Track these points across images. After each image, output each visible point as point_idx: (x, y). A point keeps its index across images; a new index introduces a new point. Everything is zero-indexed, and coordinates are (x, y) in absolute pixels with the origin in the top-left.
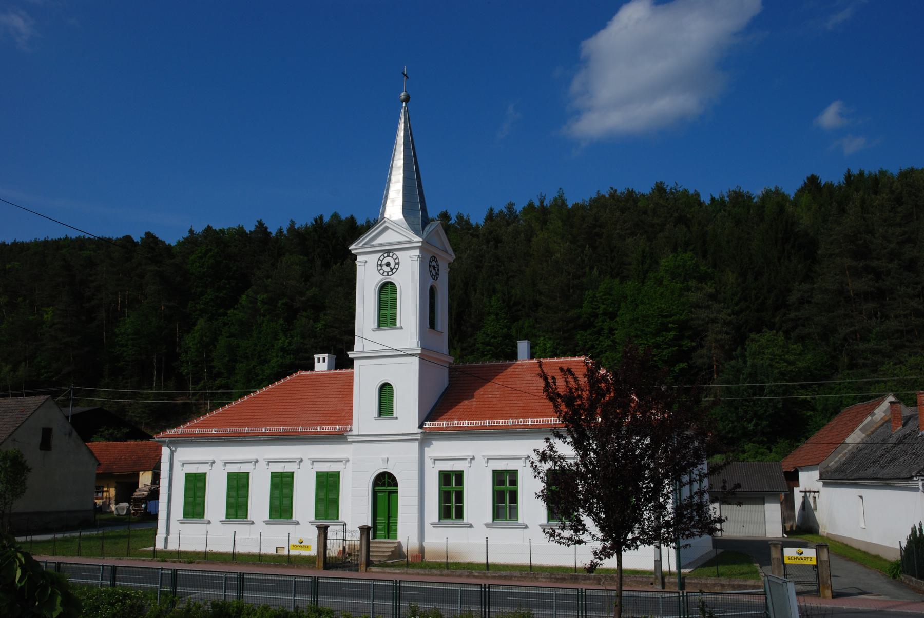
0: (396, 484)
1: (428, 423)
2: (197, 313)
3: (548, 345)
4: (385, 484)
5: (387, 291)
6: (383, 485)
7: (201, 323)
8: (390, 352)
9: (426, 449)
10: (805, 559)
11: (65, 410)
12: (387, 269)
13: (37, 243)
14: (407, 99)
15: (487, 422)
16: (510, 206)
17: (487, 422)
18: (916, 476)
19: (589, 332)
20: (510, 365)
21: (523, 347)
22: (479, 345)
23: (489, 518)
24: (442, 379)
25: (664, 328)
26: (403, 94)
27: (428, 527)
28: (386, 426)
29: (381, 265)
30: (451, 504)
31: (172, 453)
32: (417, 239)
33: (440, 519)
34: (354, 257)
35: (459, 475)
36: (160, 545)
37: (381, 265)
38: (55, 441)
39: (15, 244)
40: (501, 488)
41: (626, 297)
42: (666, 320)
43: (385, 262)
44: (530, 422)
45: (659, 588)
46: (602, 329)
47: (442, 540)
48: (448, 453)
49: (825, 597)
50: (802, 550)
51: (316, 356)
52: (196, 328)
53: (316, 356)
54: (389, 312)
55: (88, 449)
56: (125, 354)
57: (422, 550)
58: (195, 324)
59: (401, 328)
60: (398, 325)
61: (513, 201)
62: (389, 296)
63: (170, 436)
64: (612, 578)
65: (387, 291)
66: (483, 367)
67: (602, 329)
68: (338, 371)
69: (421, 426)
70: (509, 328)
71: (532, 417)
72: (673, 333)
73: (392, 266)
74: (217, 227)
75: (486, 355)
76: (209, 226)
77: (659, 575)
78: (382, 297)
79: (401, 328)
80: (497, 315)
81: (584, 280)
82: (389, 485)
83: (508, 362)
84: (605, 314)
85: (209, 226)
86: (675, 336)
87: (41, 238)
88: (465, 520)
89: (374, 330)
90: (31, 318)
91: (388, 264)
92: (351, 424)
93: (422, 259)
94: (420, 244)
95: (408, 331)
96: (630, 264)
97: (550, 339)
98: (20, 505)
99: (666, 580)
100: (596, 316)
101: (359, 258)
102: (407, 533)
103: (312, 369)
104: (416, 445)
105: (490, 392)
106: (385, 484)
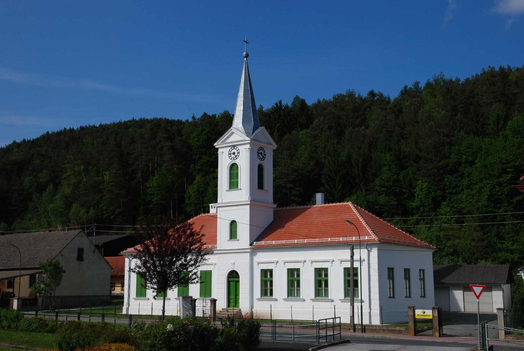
0: (239, 277)
1: (255, 242)
2: (196, 172)
3: (424, 186)
4: (233, 277)
5: (233, 167)
6: (233, 277)
7: (198, 178)
8: (233, 205)
9: (254, 257)
10: (426, 315)
11: (90, 238)
12: (233, 156)
13: (114, 125)
14: (247, 56)
15: (284, 242)
16: (417, 84)
17: (284, 242)
18: (520, 270)
19: (455, 175)
20: (309, 208)
21: (319, 196)
22: (377, 188)
23: (285, 296)
24: (268, 217)
25: (504, 171)
26: (244, 53)
27: (255, 301)
28: (234, 245)
29: (230, 154)
30: (267, 290)
31: (130, 261)
32: (248, 139)
33: (262, 296)
34: (217, 150)
35: (271, 271)
36: (124, 312)
37: (230, 154)
38: (85, 256)
39: (101, 126)
40: (265, 279)
41: (482, 150)
42: (504, 166)
43: (232, 152)
44: (306, 241)
45: (352, 331)
46: (464, 173)
47: (262, 309)
48: (265, 259)
49: (435, 336)
50: (425, 310)
51: (210, 205)
52: (195, 182)
53: (210, 205)
54: (235, 180)
55: (105, 260)
56: (153, 200)
57: (252, 313)
58: (194, 179)
59: (241, 189)
60: (239, 188)
61: (418, 81)
62: (235, 171)
63: (129, 252)
64: (344, 328)
65: (233, 167)
66: (295, 209)
67: (464, 173)
68: (327, 205)
69: (251, 244)
70: (398, 175)
71: (343, 237)
72: (510, 175)
73: (236, 154)
74: (210, 114)
75: (382, 194)
76: (205, 113)
77: (352, 324)
78: (232, 172)
79: (241, 189)
80: (390, 166)
81: (454, 139)
82: (236, 277)
83: (305, 206)
84: (466, 162)
85: (205, 113)
86: (511, 177)
87: (117, 121)
88: (274, 297)
89: (227, 191)
90: (97, 179)
91: (234, 153)
92: (216, 243)
93: (251, 150)
94: (249, 142)
95: (244, 192)
96: (490, 125)
97: (426, 182)
98: (60, 292)
99: (356, 327)
100: (460, 164)
101: (220, 150)
102: (244, 307)
103: (209, 212)
104: (248, 255)
105: (293, 225)
106: (233, 277)
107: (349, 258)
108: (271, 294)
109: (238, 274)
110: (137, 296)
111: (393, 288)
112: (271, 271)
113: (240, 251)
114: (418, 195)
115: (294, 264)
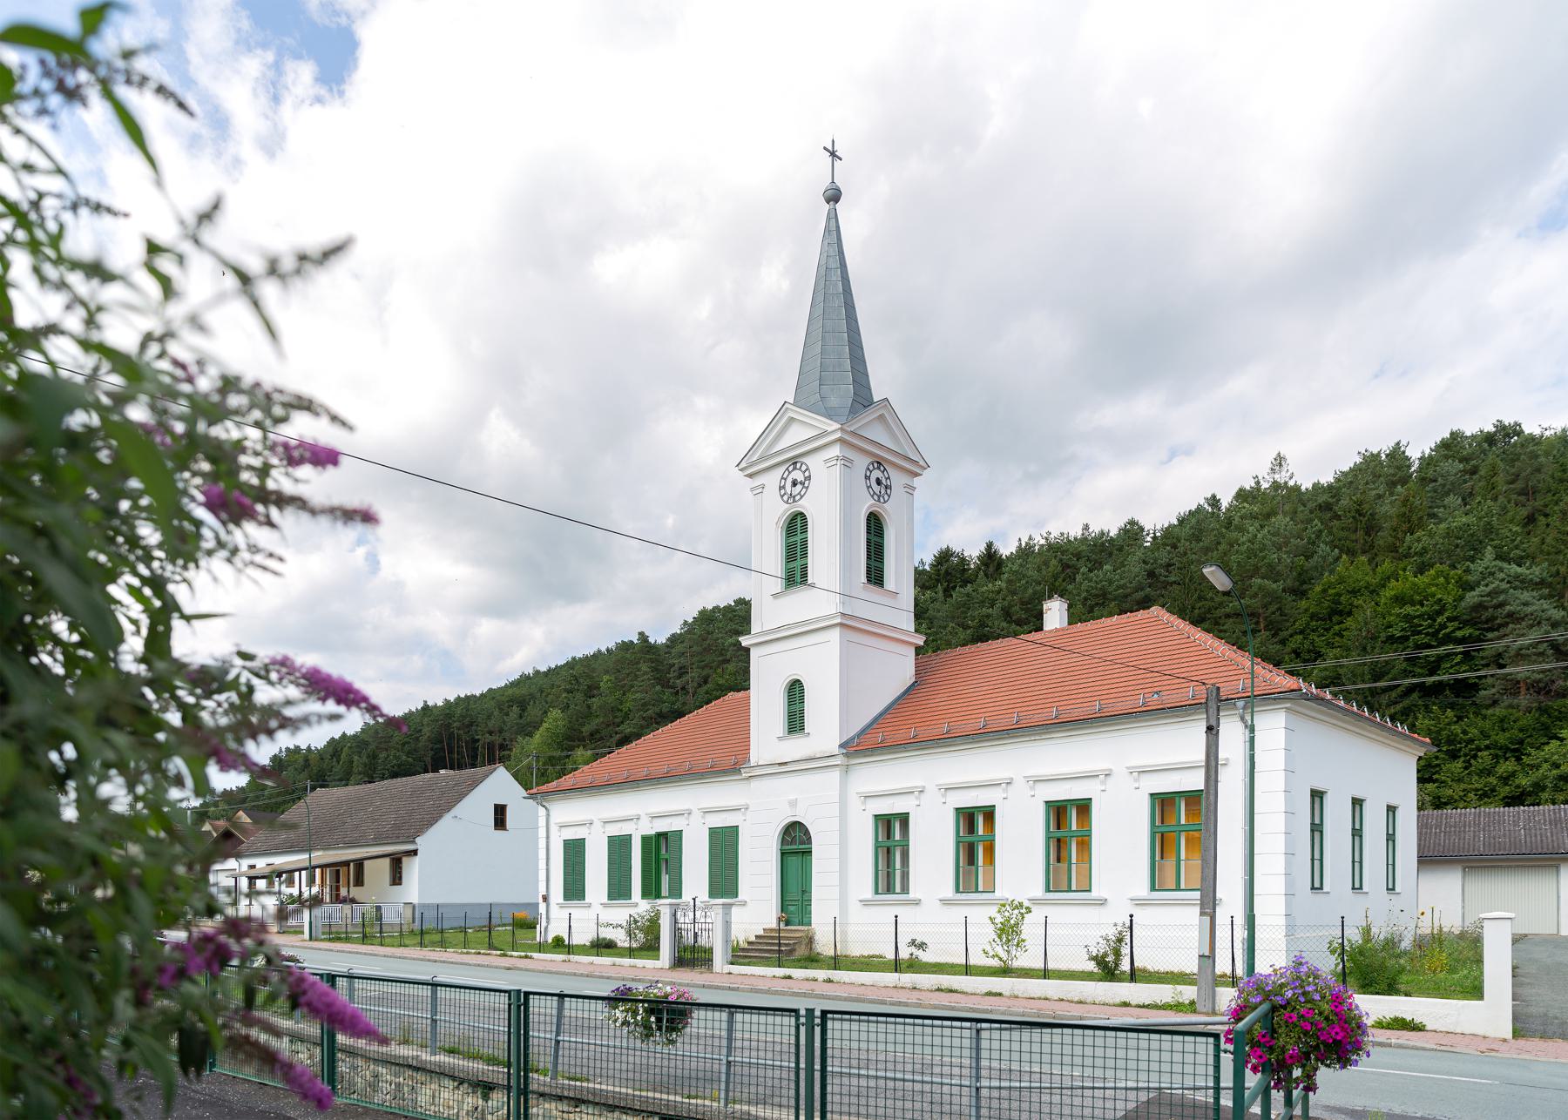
4: (795, 842)
28: (796, 748)
35: (904, 819)
43: (799, 487)
88: (911, 895)
106: (795, 842)
107: (1200, 756)
108: (905, 889)
109: (807, 832)
110: (611, 897)
111: (1321, 860)
112: (904, 819)
113: (812, 764)
114: (1501, 570)
115: (669, 820)
